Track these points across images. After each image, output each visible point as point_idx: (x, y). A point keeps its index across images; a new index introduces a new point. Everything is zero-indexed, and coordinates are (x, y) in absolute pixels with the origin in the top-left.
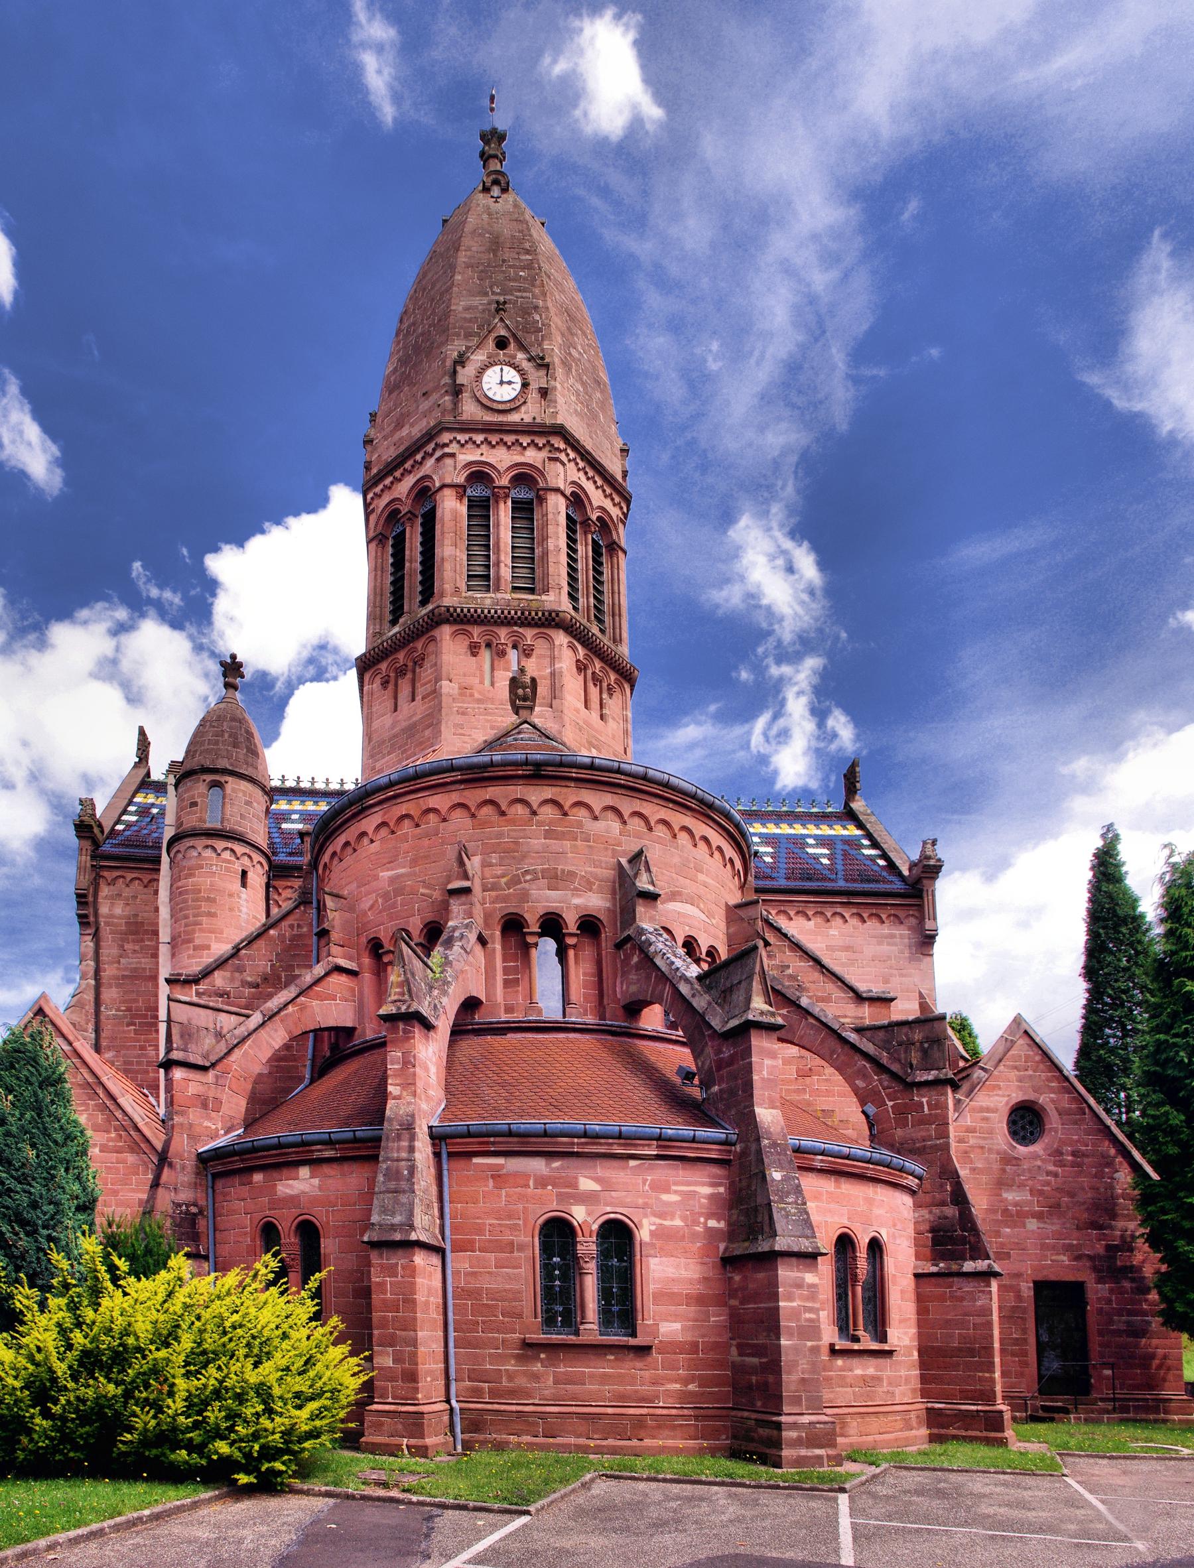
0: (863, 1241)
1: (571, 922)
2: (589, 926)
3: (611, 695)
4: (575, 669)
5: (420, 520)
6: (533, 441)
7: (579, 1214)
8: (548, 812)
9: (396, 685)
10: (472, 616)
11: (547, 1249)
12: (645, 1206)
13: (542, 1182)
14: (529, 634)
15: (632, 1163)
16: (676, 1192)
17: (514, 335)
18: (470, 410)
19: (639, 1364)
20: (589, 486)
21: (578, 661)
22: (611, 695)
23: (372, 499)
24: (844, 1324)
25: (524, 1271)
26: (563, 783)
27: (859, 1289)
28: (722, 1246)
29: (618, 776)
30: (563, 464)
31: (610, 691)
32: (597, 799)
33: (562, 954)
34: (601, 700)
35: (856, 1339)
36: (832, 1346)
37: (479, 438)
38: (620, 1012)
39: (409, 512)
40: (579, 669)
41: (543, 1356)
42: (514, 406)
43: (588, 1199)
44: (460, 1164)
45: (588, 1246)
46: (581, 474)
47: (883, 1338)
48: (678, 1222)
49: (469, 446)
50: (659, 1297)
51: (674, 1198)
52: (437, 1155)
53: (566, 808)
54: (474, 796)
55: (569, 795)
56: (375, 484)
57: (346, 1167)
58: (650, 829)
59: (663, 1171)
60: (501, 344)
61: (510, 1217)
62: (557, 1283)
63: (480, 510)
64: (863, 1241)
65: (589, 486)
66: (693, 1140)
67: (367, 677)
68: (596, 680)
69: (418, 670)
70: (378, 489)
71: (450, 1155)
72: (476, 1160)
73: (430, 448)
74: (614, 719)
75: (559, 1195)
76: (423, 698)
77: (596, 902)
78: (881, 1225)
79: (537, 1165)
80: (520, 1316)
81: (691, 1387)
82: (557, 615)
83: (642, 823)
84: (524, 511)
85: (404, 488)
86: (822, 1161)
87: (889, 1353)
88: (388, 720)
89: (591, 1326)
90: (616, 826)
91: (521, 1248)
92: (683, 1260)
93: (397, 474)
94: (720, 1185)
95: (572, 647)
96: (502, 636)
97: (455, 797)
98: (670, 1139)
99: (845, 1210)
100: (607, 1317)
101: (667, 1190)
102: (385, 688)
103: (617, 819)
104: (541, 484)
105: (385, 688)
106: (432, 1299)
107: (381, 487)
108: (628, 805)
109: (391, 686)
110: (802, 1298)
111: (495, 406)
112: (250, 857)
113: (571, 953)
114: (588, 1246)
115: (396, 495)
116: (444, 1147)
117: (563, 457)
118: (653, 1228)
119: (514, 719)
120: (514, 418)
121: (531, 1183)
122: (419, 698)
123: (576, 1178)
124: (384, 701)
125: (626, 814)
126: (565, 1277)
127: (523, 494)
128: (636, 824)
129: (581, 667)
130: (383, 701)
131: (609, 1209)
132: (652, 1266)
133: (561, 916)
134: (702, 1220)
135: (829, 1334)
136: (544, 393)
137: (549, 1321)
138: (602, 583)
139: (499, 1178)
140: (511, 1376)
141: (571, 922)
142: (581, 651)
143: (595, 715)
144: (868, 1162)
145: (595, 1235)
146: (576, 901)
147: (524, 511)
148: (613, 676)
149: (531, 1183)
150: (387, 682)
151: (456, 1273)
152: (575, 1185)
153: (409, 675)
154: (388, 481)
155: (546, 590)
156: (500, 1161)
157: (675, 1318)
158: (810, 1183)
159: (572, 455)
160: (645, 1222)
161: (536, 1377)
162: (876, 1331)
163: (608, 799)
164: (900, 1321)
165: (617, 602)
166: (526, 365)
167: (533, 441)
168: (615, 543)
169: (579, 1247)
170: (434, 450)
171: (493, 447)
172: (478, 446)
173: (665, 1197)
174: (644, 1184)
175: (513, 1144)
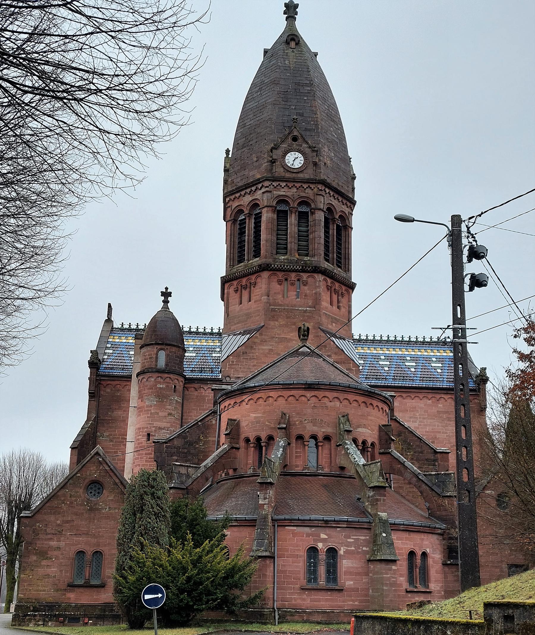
0: (419, 553)
1: (320, 437)
2: (327, 438)
3: (343, 297)
4: (326, 289)
5: (254, 216)
6: (309, 186)
7: (320, 545)
8: (314, 400)
9: (241, 292)
10: (279, 268)
11: (309, 557)
12: (342, 543)
13: (308, 535)
14: (305, 276)
15: (338, 529)
16: (352, 539)
17: (302, 136)
18: (279, 171)
19: (339, 596)
20: (335, 203)
21: (327, 286)
22: (343, 297)
23: (229, 201)
24: (411, 580)
25: (301, 564)
26: (319, 390)
27: (418, 570)
28: (367, 556)
29: (339, 387)
30: (323, 196)
31: (342, 295)
32: (331, 395)
33: (317, 446)
34: (338, 299)
35: (416, 587)
36: (406, 589)
37: (283, 184)
38: (338, 469)
39: (249, 213)
40: (328, 289)
41: (306, 593)
42: (300, 171)
43: (323, 541)
44: (280, 529)
45: (322, 556)
46: (332, 198)
47: (428, 587)
48: (353, 548)
49: (279, 187)
50: (346, 573)
51: (352, 540)
52: (274, 526)
53: (320, 398)
54: (287, 393)
55: (320, 394)
56: (232, 195)
57: (241, 529)
58: (351, 404)
59: (348, 531)
60: (295, 139)
61: (297, 547)
62: (312, 568)
63: (282, 216)
64: (419, 553)
65: (335, 203)
66: (358, 522)
67: (227, 286)
68: (336, 292)
69: (252, 288)
70: (232, 197)
71: (278, 526)
72: (286, 528)
73: (260, 186)
74: (344, 307)
75: (314, 539)
76: (255, 302)
77: (329, 430)
78: (427, 548)
79: (307, 529)
80: (299, 579)
81: (356, 603)
82: (319, 268)
83: (348, 402)
84: (303, 217)
85: (247, 199)
86: (403, 527)
87: (430, 592)
88: (237, 308)
89: (322, 582)
90: (338, 403)
91: (300, 557)
92: (354, 561)
93: (243, 193)
94: (367, 536)
95: (325, 280)
96: (293, 277)
97: (280, 393)
98: (351, 522)
99: (412, 543)
100: (328, 580)
101: (350, 538)
102: (236, 293)
103: (338, 401)
104: (313, 206)
105: (236, 293)
106: (270, 574)
107: (233, 196)
108: (342, 396)
109: (239, 292)
110: (391, 574)
111: (291, 170)
112: (177, 380)
113: (320, 448)
114: (322, 556)
115: (242, 203)
116: (276, 523)
117: (323, 193)
118: (344, 550)
119: (300, 344)
120: (301, 175)
121: (305, 536)
122: (252, 301)
123: (320, 534)
124: (235, 299)
125: (341, 399)
126: (315, 566)
127: (304, 209)
128: (346, 402)
129: (329, 288)
130: (234, 297)
131: (330, 544)
132: (344, 563)
133: (317, 436)
134: (361, 547)
135: (405, 585)
136: (315, 164)
137: (309, 581)
138: (341, 244)
139: (294, 534)
140: (295, 599)
141: (320, 437)
142: (329, 280)
143: (335, 308)
144: (421, 527)
145: (325, 552)
146: (323, 430)
147: (303, 217)
148: (344, 288)
149: (305, 536)
150: (237, 290)
151: (278, 565)
152: (320, 537)
153: (248, 290)
154: (237, 195)
155: (313, 256)
156: (295, 528)
157: (351, 580)
158: (394, 536)
159: (327, 191)
160: (342, 548)
161: (304, 600)
162: (425, 584)
163: (335, 394)
164: (435, 581)
165: (347, 252)
166: (308, 151)
167: (309, 186)
168: (347, 225)
169: (320, 556)
170: (261, 188)
171: (290, 188)
172: (283, 188)
173: (349, 540)
174: (342, 536)
175: (299, 523)
